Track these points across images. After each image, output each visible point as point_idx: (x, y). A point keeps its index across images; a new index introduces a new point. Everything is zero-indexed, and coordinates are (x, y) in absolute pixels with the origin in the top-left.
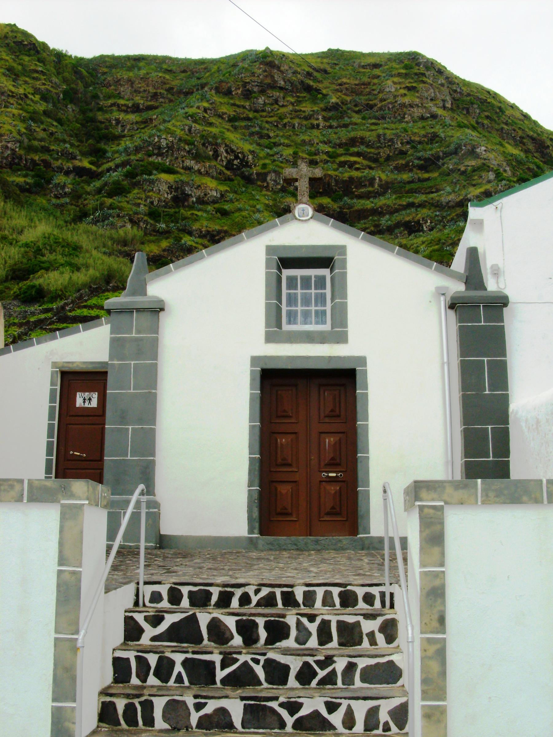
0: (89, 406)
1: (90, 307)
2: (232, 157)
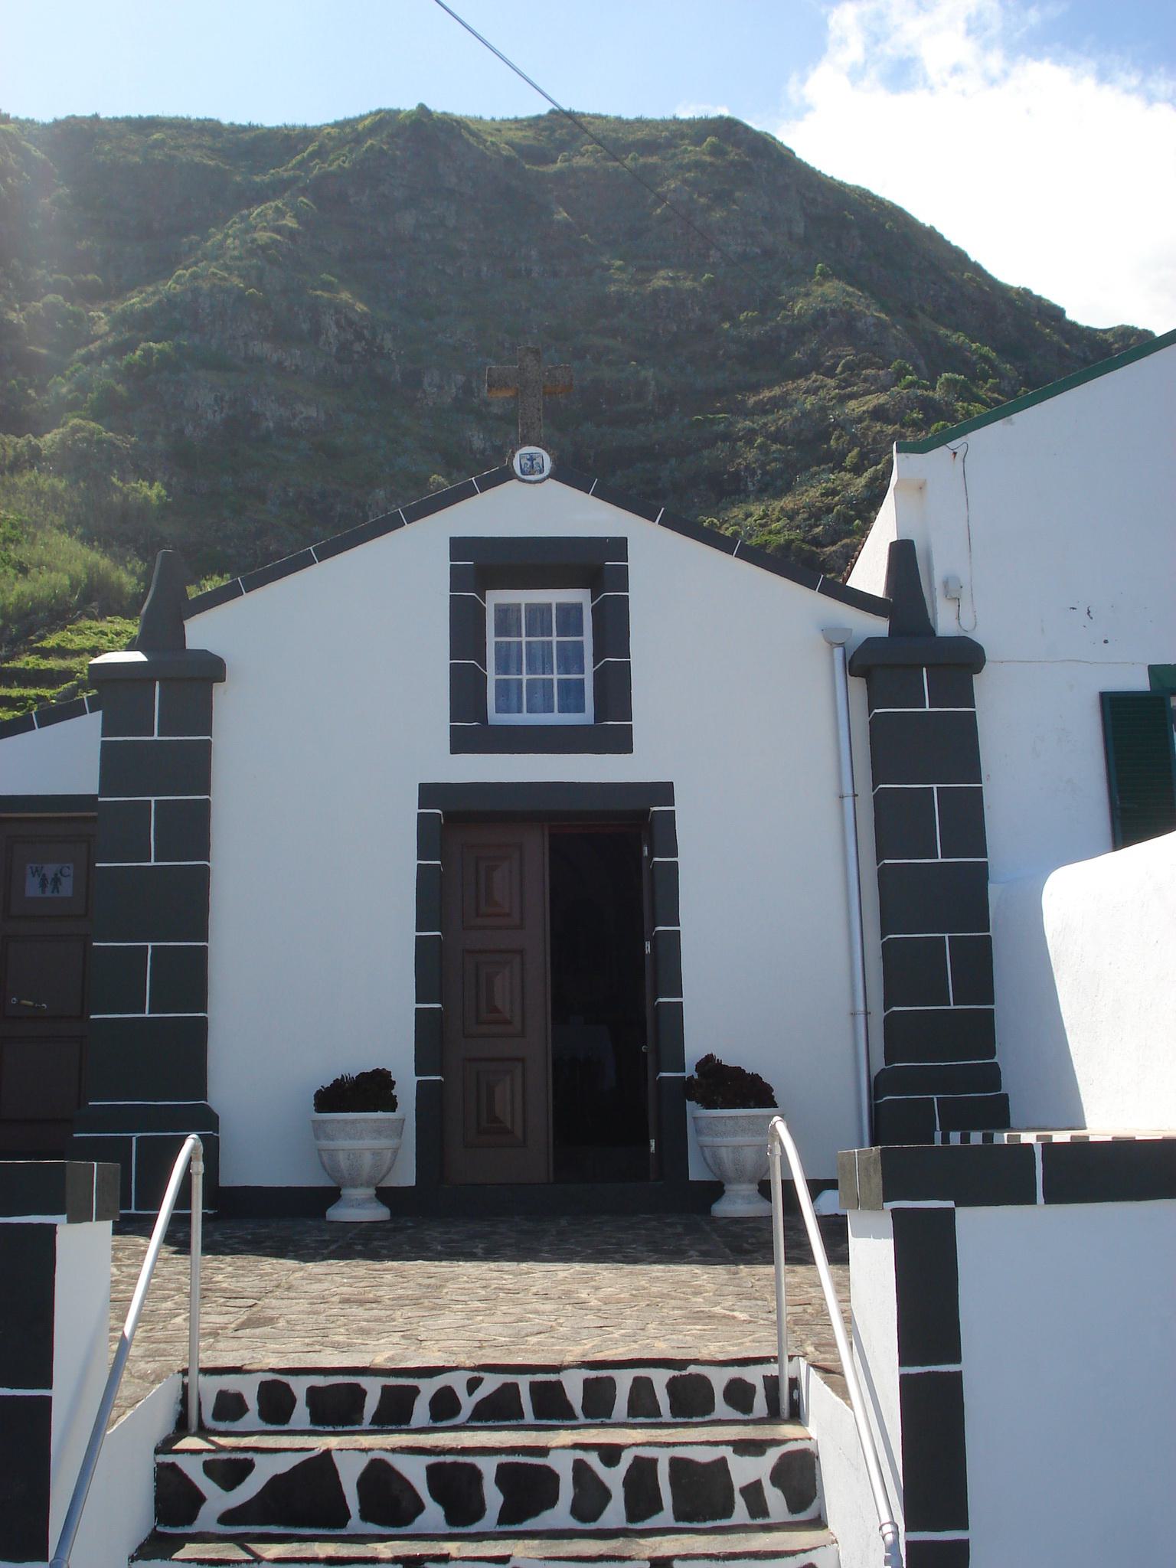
0: (56, 894)
1: (45, 653)
2: (350, 337)
